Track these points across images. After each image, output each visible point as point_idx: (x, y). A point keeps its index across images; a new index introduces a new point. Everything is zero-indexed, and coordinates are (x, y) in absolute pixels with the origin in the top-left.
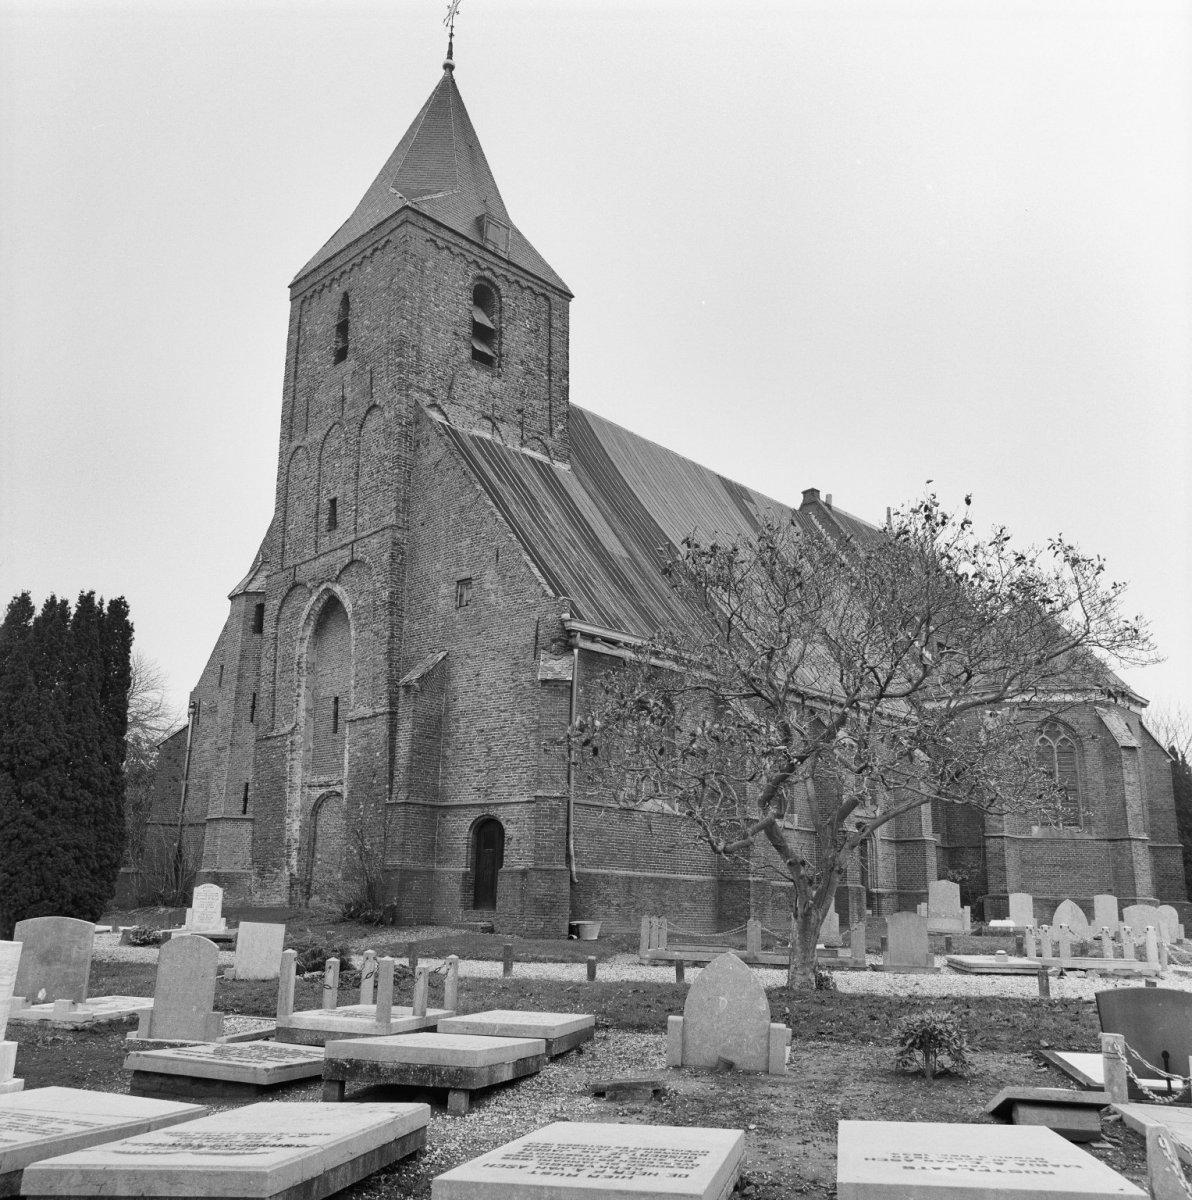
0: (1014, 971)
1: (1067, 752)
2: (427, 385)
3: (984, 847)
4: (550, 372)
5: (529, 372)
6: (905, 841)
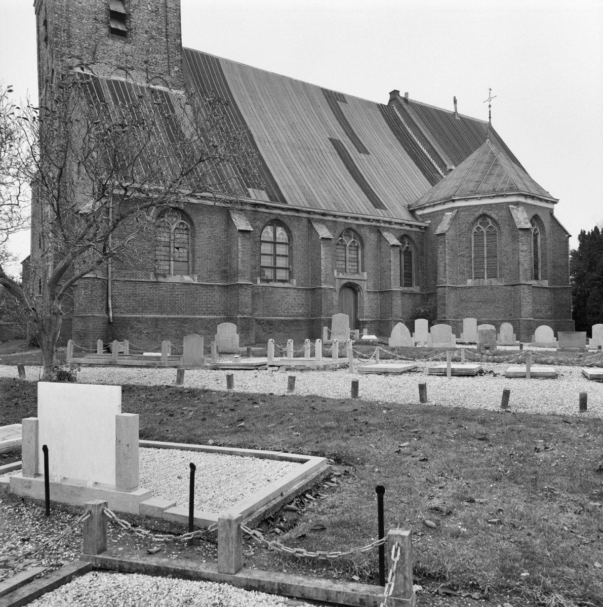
0: (240, 368)
1: (492, 234)
2: (77, 53)
3: (436, 293)
4: (167, 36)
5: (152, 37)
6: (384, 292)
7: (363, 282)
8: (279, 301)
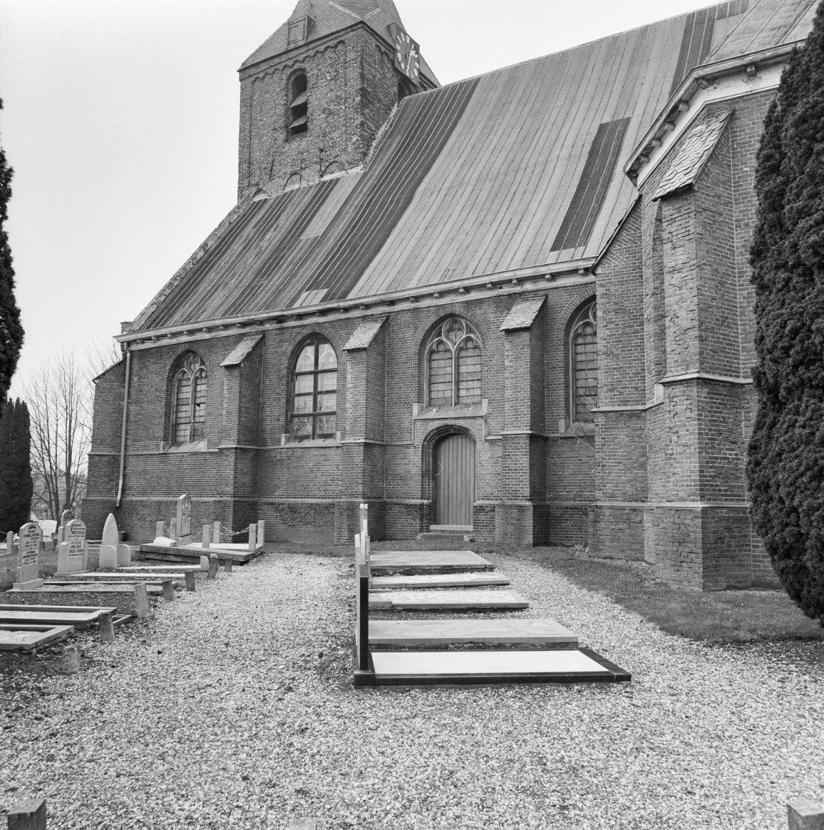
7: (478, 421)
8: (312, 471)
